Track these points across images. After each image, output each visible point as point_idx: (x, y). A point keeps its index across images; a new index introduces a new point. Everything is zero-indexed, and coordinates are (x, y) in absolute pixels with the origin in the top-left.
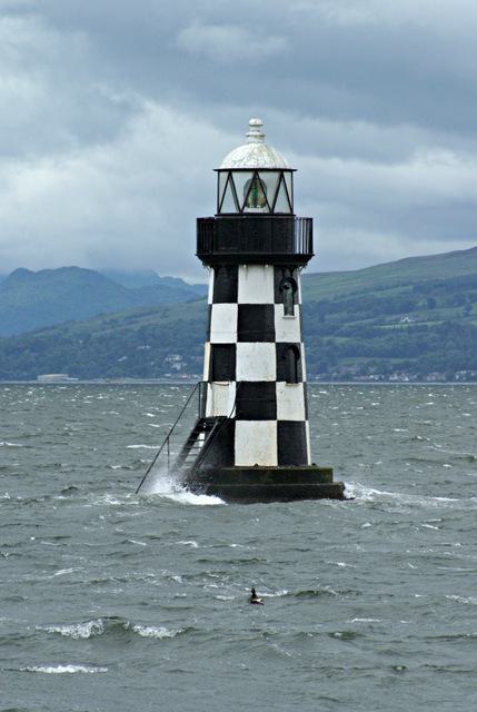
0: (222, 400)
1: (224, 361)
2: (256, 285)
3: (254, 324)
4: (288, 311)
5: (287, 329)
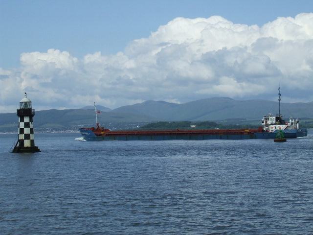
0: (22, 137)
1: (22, 131)
2: (27, 120)
3: (27, 125)
4: (32, 123)
5: (31, 126)
